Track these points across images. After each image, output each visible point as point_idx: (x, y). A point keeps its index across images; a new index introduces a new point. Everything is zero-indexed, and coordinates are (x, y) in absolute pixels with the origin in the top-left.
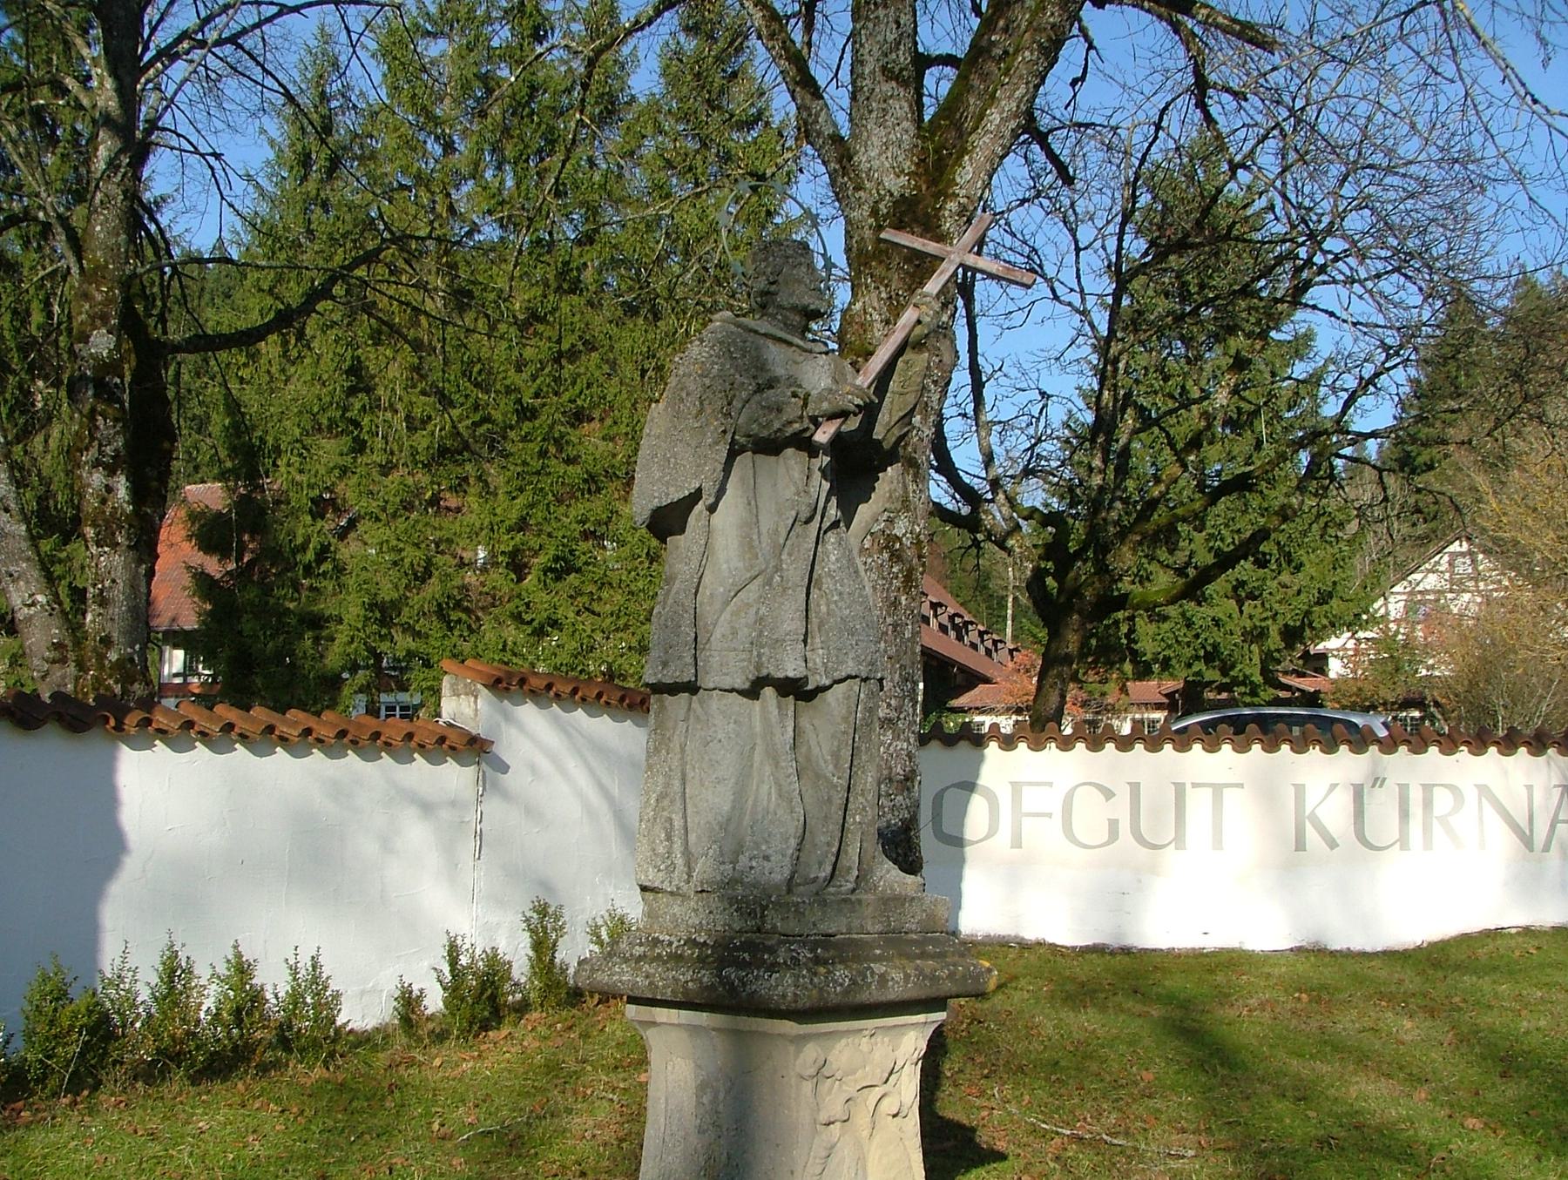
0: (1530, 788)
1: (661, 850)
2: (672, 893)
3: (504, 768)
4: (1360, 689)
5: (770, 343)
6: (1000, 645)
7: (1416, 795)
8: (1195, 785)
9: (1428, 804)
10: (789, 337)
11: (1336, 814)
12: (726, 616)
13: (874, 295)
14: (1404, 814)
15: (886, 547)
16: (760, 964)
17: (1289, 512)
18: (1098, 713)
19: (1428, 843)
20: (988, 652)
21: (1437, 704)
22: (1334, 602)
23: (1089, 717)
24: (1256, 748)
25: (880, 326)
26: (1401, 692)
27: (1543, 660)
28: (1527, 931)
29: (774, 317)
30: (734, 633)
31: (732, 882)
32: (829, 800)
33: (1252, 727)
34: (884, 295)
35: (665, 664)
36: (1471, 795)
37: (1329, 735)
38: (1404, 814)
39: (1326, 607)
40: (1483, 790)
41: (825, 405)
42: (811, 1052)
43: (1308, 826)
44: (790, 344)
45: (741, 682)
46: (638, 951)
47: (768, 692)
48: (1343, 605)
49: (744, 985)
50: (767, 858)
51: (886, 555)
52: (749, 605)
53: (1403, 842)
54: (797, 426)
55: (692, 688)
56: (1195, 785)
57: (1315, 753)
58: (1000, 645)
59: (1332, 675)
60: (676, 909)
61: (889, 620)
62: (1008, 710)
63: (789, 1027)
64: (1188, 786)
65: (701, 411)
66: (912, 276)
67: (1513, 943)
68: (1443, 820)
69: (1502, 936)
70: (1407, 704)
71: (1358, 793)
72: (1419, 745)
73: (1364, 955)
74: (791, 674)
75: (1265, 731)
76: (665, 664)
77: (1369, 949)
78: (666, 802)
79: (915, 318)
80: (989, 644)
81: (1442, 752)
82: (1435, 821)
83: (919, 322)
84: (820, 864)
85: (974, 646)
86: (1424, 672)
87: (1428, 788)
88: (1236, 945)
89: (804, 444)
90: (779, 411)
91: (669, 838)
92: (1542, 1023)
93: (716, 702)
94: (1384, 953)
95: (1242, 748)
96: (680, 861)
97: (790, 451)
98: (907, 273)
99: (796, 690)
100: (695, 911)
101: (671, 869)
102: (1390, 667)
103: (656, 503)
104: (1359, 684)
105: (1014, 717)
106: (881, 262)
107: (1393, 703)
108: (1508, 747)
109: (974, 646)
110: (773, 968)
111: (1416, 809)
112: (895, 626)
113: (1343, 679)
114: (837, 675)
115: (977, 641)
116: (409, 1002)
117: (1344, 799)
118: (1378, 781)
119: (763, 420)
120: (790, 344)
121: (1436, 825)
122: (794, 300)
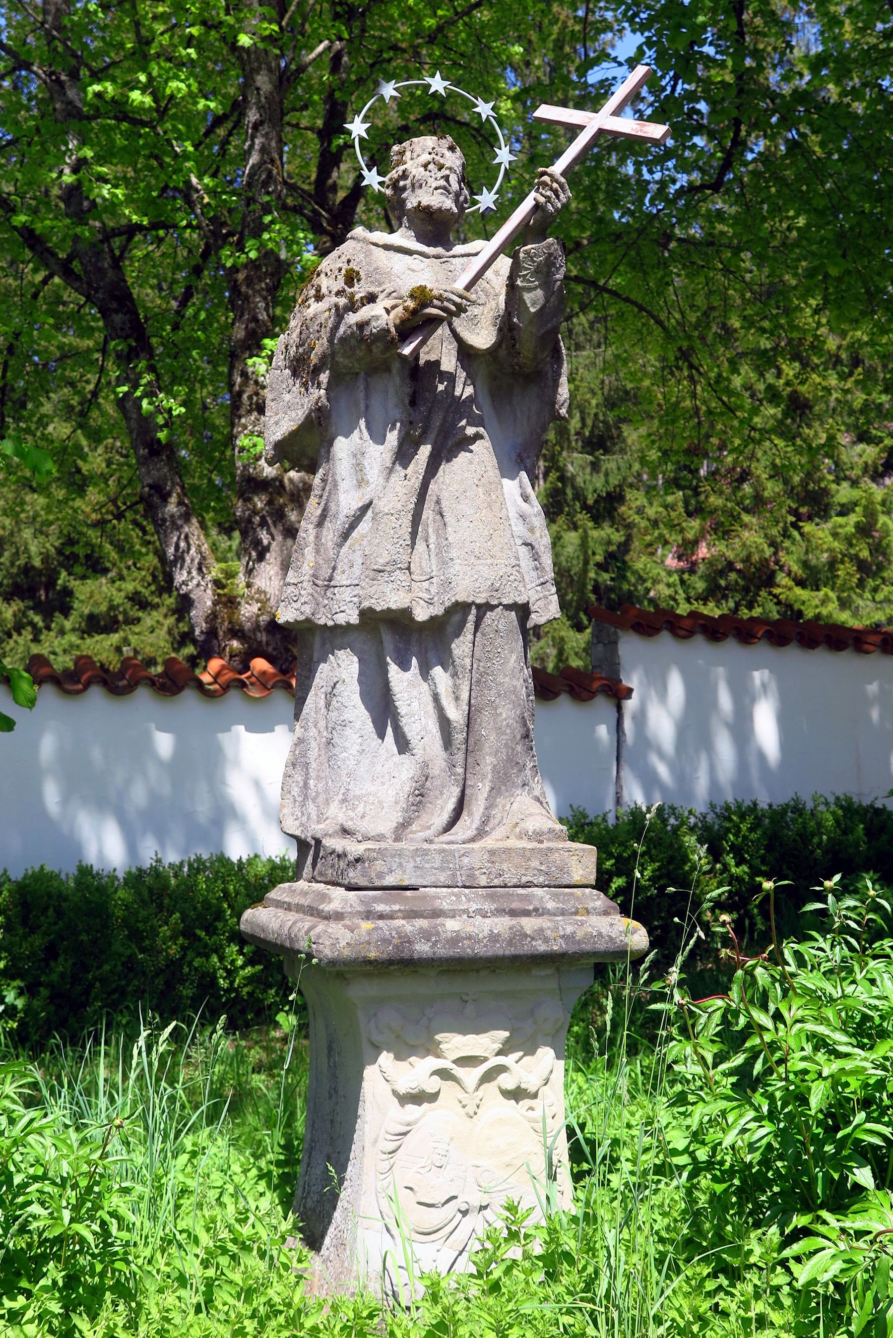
74: (394, 607)
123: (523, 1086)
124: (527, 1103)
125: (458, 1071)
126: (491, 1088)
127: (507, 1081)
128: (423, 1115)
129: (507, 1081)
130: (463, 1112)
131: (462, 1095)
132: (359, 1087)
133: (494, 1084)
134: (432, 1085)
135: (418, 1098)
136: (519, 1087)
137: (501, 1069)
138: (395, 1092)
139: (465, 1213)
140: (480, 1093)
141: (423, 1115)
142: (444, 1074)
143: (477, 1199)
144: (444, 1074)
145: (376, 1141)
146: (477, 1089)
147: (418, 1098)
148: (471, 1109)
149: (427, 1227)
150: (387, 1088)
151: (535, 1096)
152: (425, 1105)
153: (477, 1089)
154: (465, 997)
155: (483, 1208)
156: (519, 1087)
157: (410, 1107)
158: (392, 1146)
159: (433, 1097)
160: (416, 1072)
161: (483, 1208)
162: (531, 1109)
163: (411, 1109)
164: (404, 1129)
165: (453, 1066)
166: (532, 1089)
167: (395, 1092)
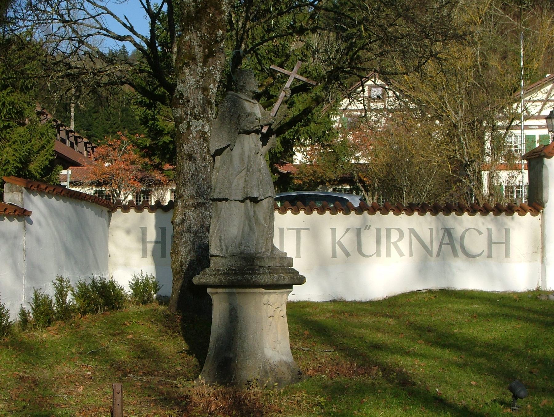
0: (431, 230)
1: (218, 245)
2: (222, 257)
3: (31, 222)
4: (315, 172)
5: (245, 101)
6: (79, 140)
7: (383, 233)
8: (288, 229)
9: (388, 236)
10: (248, 99)
11: (347, 240)
12: (236, 180)
13: (194, 35)
14: (378, 242)
15: (202, 137)
16: (256, 274)
17: (321, 99)
18: (150, 186)
19: (388, 255)
20: (72, 145)
21: (361, 181)
22: (312, 125)
23: (143, 188)
24: (302, 212)
25: (197, 47)
26: (339, 173)
27: (429, 162)
28: (430, 291)
29: (245, 93)
30: (239, 185)
31: (242, 253)
32: (263, 230)
33: (299, 203)
34: (199, 35)
35: (220, 193)
36: (407, 233)
37: (345, 207)
38: (378, 242)
39: (308, 128)
40: (412, 231)
41: (265, 122)
42: (266, 297)
43: (338, 247)
44: (251, 102)
45: (241, 198)
46: (213, 273)
47: (248, 201)
48: (317, 127)
49: (252, 279)
50: (249, 247)
51: (202, 140)
52: (242, 177)
53: (378, 254)
54: (257, 128)
55: (226, 200)
56: (288, 229)
57: (340, 214)
58: (79, 140)
59: (297, 162)
60: (223, 261)
61: (203, 165)
62: (92, 184)
63: (262, 290)
64: (285, 230)
65: (230, 122)
66: (210, 28)
67: (425, 296)
68: (395, 244)
69: (420, 293)
70: (343, 181)
71: (359, 232)
72: (385, 211)
73: (361, 303)
75: (305, 204)
76: (220, 193)
77: (363, 300)
78: (219, 231)
79: (284, 95)
80: (72, 139)
81: (395, 214)
82: (391, 245)
83: (285, 96)
84: (261, 248)
85: (63, 141)
86: (353, 161)
87: (388, 230)
88: (307, 300)
89: (257, 132)
90: (253, 123)
91: (220, 241)
92: (440, 318)
93: (233, 204)
94: (370, 302)
95: (296, 212)
96: (224, 248)
97: (253, 134)
98: (208, 26)
99: (255, 200)
100: (230, 261)
101: (222, 250)
102: (334, 157)
103: (217, 148)
104: (315, 169)
105: (94, 189)
106: (198, 22)
107: (335, 181)
108: (422, 212)
109: (63, 141)
110: (260, 274)
111: (383, 240)
112: (205, 167)
113: (303, 165)
114: (266, 196)
115: (65, 137)
116: (23, 314)
117: (351, 236)
118: (367, 227)
119: (248, 126)
120: (251, 102)
121: (392, 248)
122: (251, 89)
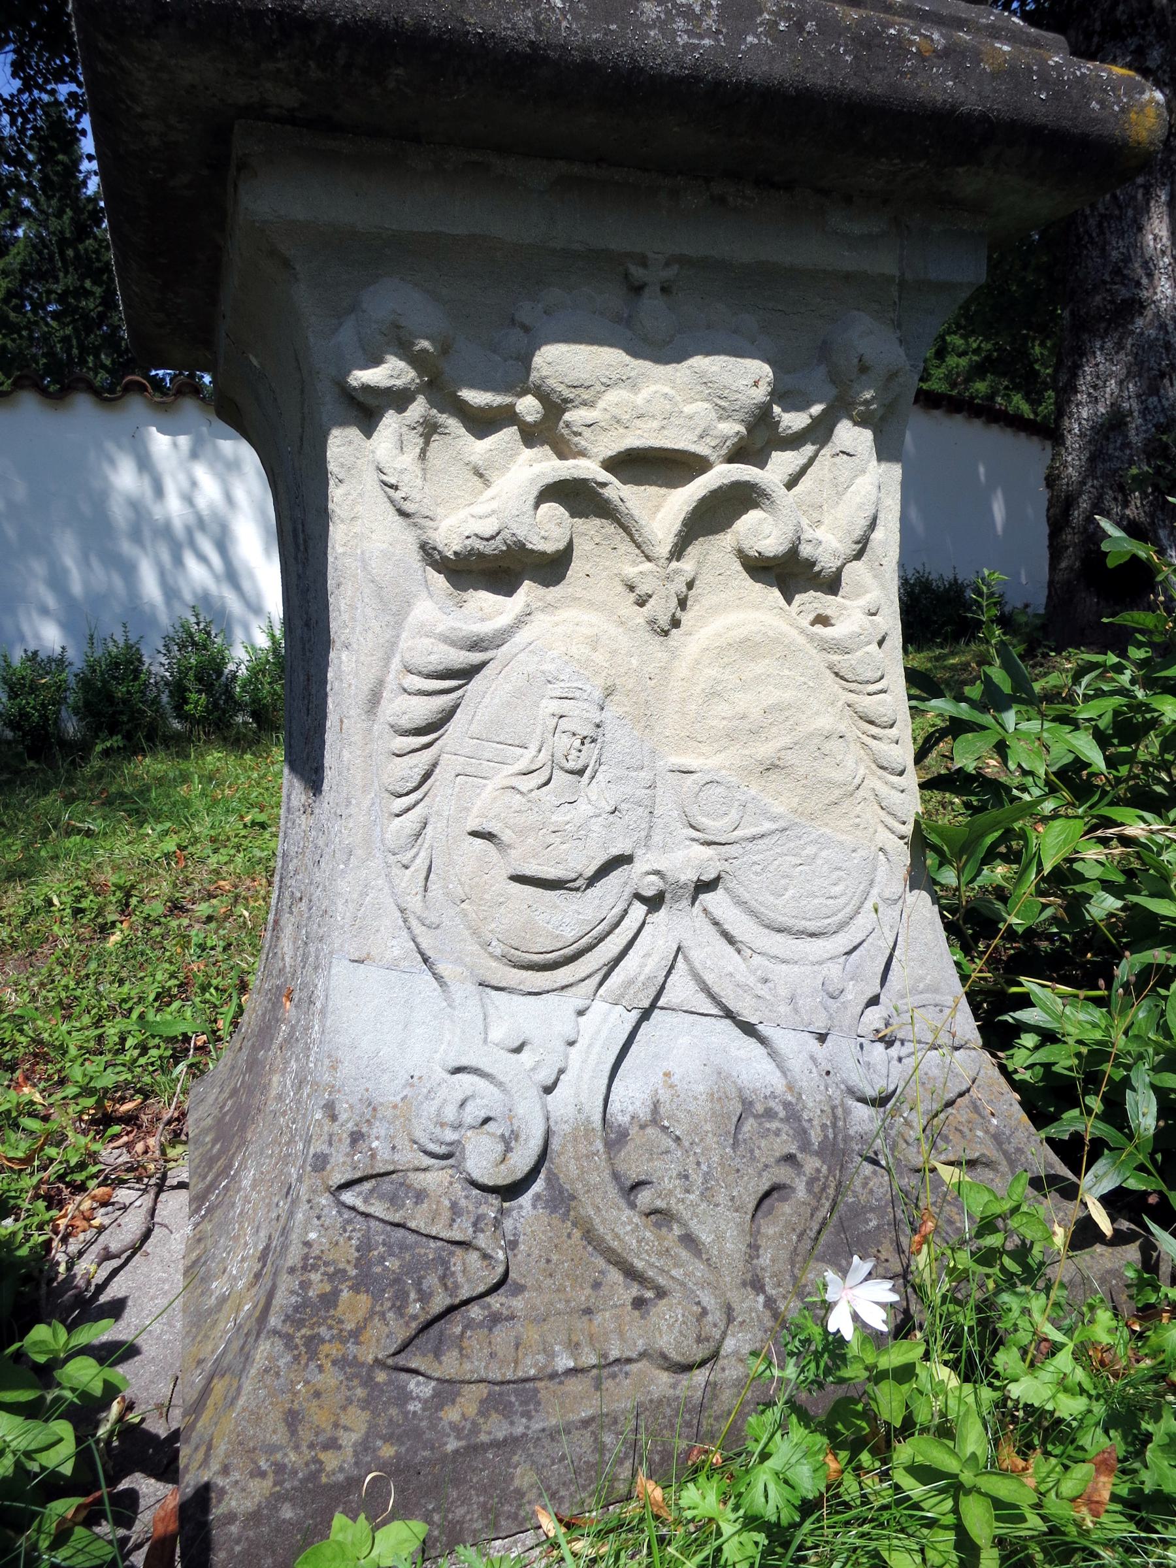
123: (806, 551)
124: (811, 601)
125: (617, 490)
126: (717, 553)
127: (760, 531)
128: (520, 622)
129: (760, 531)
130: (639, 616)
131: (636, 569)
132: (324, 496)
133: (727, 540)
134: (549, 528)
135: (497, 568)
136: (793, 552)
137: (741, 498)
138: (431, 556)
139: (654, 903)
140: (687, 566)
141: (520, 622)
142: (576, 496)
143: (686, 861)
144: (576, 496)
145: (374, 699)
146: (678, 552)
147: (497, 568)
148: (661, 608)
149: (541, 945)
150: (406, 540)
151: (832, 584)
152: (528, 591)
153: (678, 552)
154: (637, 272)
155: (704, 887)
156: (793, 552)
157: (483, 599)
158: (423, 709)
159: (552, 568)
160: (496, 488)
161: (704, 887)
162: (822, 620)
163: (487, 610)
164: (462, 658)
165: (604, 476)
166: (827, 562)
167: (431, 556)
